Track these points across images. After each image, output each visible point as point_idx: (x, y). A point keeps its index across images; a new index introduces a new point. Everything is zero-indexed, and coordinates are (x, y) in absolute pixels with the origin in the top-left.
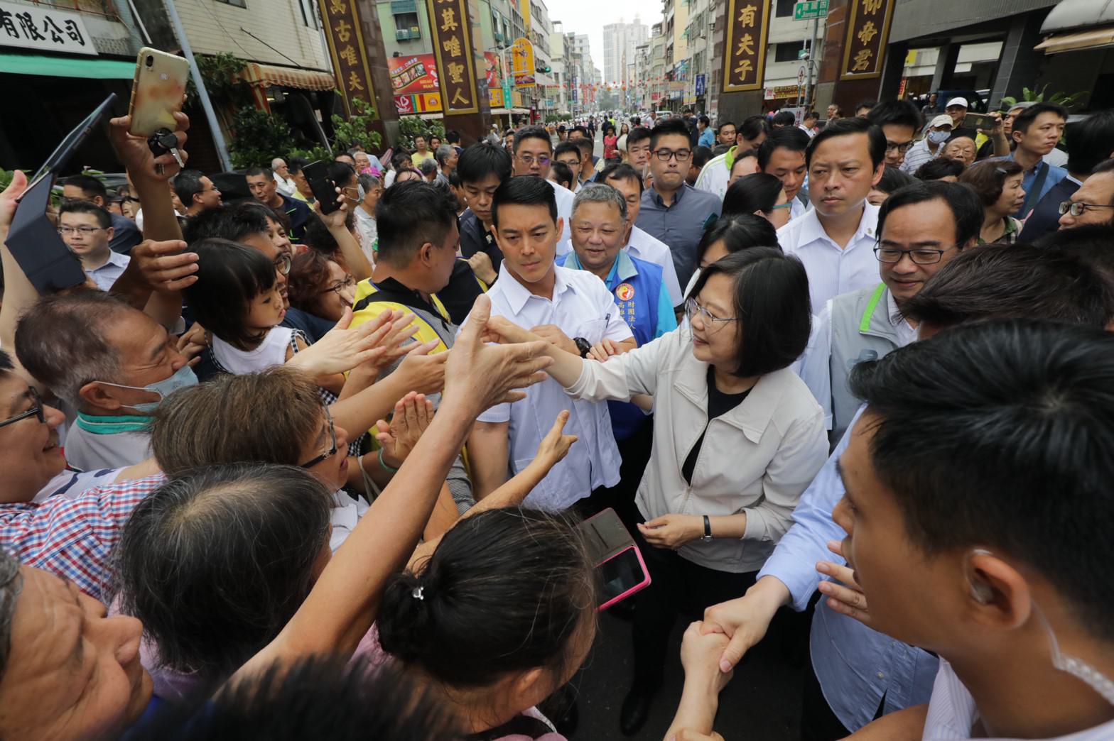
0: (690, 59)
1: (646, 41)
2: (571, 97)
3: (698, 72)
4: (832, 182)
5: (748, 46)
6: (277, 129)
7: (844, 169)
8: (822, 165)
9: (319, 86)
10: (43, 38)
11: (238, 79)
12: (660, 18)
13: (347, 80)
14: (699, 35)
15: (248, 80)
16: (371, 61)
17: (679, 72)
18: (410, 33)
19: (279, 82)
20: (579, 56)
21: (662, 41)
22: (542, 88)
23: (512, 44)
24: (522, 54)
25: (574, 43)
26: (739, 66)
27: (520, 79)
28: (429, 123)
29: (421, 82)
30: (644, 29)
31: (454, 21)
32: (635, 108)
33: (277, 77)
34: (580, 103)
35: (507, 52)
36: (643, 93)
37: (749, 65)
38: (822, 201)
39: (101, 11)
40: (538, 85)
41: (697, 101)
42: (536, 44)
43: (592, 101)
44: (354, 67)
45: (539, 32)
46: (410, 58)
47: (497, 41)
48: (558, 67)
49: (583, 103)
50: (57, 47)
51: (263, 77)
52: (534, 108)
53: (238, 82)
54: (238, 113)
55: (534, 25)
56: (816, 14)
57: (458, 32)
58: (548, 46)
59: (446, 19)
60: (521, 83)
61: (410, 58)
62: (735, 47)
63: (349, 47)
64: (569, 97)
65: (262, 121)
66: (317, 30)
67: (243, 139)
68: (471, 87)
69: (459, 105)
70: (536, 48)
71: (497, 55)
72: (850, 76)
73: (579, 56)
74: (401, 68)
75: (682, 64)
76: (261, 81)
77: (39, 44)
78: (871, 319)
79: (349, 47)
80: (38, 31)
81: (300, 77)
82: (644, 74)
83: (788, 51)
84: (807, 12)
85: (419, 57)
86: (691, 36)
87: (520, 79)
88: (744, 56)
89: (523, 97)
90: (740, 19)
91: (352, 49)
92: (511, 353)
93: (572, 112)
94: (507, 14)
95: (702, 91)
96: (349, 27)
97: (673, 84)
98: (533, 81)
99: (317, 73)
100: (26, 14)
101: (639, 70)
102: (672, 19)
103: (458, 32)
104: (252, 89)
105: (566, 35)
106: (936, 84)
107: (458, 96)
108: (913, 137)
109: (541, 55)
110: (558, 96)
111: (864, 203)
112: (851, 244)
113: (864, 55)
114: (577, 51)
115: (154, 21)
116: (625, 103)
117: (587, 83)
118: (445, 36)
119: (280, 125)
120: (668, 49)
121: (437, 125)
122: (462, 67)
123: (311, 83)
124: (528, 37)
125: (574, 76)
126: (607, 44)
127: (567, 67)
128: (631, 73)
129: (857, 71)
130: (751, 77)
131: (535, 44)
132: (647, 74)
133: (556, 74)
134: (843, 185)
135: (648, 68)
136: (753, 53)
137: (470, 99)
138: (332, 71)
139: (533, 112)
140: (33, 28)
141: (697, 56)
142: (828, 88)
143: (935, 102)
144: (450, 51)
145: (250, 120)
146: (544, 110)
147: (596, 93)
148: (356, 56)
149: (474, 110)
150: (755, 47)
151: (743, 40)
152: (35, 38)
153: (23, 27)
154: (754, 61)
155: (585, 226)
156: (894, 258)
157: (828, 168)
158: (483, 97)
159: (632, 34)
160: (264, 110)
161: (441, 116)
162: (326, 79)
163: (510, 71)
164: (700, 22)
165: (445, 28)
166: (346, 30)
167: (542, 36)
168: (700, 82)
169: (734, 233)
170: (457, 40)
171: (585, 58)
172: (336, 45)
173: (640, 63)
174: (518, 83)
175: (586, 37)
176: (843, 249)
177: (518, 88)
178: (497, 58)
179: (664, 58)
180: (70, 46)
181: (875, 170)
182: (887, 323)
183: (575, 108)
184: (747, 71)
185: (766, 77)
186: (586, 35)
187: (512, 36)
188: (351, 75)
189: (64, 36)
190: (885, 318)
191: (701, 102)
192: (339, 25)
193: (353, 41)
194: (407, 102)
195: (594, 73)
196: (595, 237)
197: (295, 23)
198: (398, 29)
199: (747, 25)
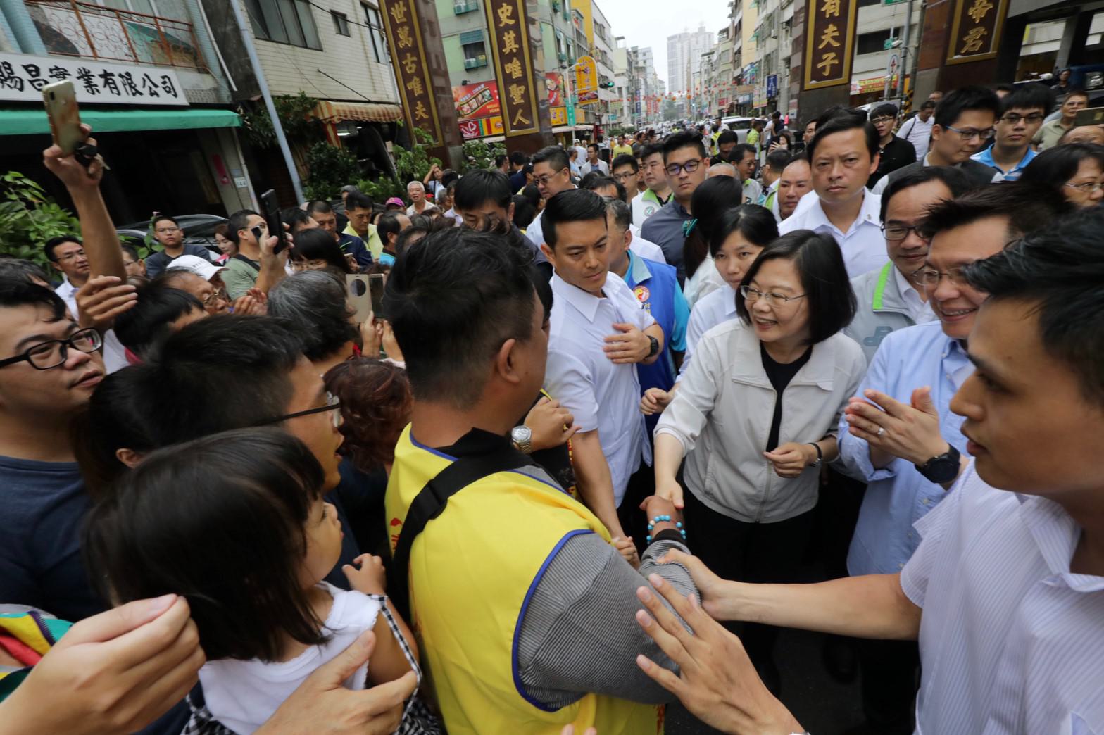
0: (760, 61)
1: (712, 47)
2: (635, 110)
3: (768, 74)
4: (835, 172)
5: (833, 38)
6: (347, 162)
7: (846, 160)
8: (825, 159)
9: (387, 118)
10: (141, 94)
11: (312, 117)
12: (727, 23)
13: (413, 110)
14: (770, 35)
15: (321, 118)
16: (436, 90)
18: (477, 61)
19: (349, 117)
20: (643, 69)
21: (729, 45)
22: (605, 103)
23: (575, 62)
24: (585, 71)
25: (637, 56)
27: (583, 97)
28: (492, 145)
29: (488, 107)
30: (710, 36)
31: (515, 43)
33: (348, 113)
34: (644, 115)
35: (571, 71)
36: (710, 100)
37: (834, 58)
38: (827, 190)
39: (193, 65)
40: (601, 100)
41: (768, 103)
42: (599, 61)
43: (655, 112)
44: (421, 98)
46: (479, 84)
47: (561, 61)
48: (621, 82)
49: (647, 114)
51: (335, 113)
52: (598, 124)
53: (312, 120)
54: (310, 149)
55: (598, 42)
57: (519, 54)
58: (611, 62)
60: (584, 100)
61: (479, 84)
62: (818, 40)
63: (415, 78)
64: (633, 109)
65: (332, 155)
67: (315, 174)
68: (532, 107)
70: (599, 65)
71: (561, 74)
73: (643, 69)
74: (469, 95)
76: (332, 117)
78: (883, 297)
79: (415, 78)
80: (137, 88)
81: (370, 111)
82: (710, 81)
83: (873, 42)
85: (486, 83)
86: (761, 36)
87: (583, 97)
88: (829, 48)
89: (586, 113)
90: (823, 9)
91: (418, 79)
92: (563, 419)
93: (636, 124)
94: (571, 34)
95: (773, 93)
96: (415, 59)
97: (741, 88)
98: (596, 97)
99: (387, 106)
100: (128, 74)
101: (705, 77)
102: (740, 22)
103: (519, 54)
104: (325, 126)
105: (630, 50)
106: (1061, 62)
107: (519, 117)
108: (993, 122)
109: (604, 71)
110: (622, 110)
111: (864, 190)
112: (852, 229)
113: (975, 35)
114: (641, 64)
115: (240, 70)
116: (690, 112)
117: (651, 96)
118: (506, 59)
119: (348, 159)
120: (736, 53)
121: (499, 148)
122: (523, 88)
124: (591, 55)
125: (637, 89)
126: (671, 54)
127: (630, 80)
128: (696, 82)
129: (967, 53)
130: (837, 71)
131: (598, 61)
132: (713, 80)
133: (620, 89)
134: (845, 175)
135: (714, 74)
136: (838, 45)
138: (400, 102)
139: (597, 127)
141: (768, 57)
142: (930, 76)
143: (1066, 81)
144: (511, 73)
145: (321, 155)
146: (607, 125)
147: (660, 104)
149: (535, 130)
150: (841, 38)
151: (826, 31)
152: (134, 94)
153: (124, 85)
154: (840, 53)
156: (901, 236)
157: (831, 161)
158: (543, 116)
159: (697, 43)
160: (336, 144)
161: (502, 138)
162: (394, 111)
163: (573, 89)
164: (770, 22)
166: (413, 62)
167: (605, 53)
168: (772, 84)
169: (746, 221)
171: (648, 70)
172: (403, 78)
174: (581, 100)
176: (845, 233)
177: (582, 105)
178: (561, 77)
181: (872, 161)
182: (899, 299)
183: (639, 121)
184: (832, 66)
185: (854, 71)
186: (649, 48)
187: (575, 55)
188: (417, 105)
189: (160, 91)
190: (897, 295)
191: (772, 103)
192: (406, 58)
195: (658, 84)
197: (368, 61)
198: (467, 58)
199: (832, 14)
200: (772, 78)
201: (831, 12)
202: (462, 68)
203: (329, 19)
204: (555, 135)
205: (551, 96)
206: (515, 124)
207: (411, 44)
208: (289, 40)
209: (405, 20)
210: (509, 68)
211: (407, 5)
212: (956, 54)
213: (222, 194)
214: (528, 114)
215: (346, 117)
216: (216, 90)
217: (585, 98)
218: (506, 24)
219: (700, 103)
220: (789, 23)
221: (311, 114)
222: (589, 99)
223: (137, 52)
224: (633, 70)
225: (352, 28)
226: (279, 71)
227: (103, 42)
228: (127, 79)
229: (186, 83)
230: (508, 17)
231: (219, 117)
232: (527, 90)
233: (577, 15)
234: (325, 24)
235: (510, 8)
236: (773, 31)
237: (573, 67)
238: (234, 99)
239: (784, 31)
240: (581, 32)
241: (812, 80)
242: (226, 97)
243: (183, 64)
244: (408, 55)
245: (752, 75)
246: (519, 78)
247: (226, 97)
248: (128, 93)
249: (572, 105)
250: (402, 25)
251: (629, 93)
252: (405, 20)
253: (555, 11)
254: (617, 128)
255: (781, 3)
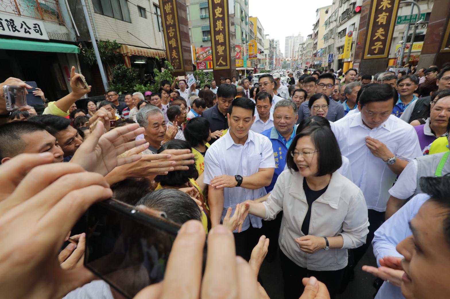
2: (271, 63)
3: (329, 53)
5: (382, 35)
10: (19, 31)
11: (118, 52)
12: (311, 32)
14: (331, 38)
15: (122, 53)
17: (320, 53)
20: (275, 48)
21: (311, 41)
22: (259, 60)
23: (249, 42)
24: (253, 46)
25: (273, 43)
26: (374, 45)
31: (222, 26)
32: (297, 68)
34: (274, 66)
35: (246, 45)
36: (302, 62)
39: (57, 21)
40: (258, 59)
44: (175, 48)
45: (260, 38)
47: (243, 41)
48: (267, 52)
49: (276, 66)
50: (27, 35)
51: (129, 51)
52: (256, 68)
55: (258, 35)
56: (409, 21)
58: (263, 44)
59: (218, 25)
60: (251, 57)
62: (373, 35)
63: (173, 39)
64: (270, 63)
66: (160, 31)
69: (221, 65)
70: (258, 44)
71: (242, 46)
72: (446, 50)
74: (203, 51)
75: (321, 50)
76: (128, 53)
77: (16, 34)
79: (173, 39)
82: (302, 55)
84: (404, 20)
86: (326, 38)
87: (251, 56)
88: (378, 40)
89: (251, 63)
90: (377, 20)
91: (174, 40)
93: (271, 69)
96: (174, 30)
98: (256, 57)
100: (11, 20)
101: (300, 53)
102: (317, 32)
104: (124, 57)
105: (271, 40)
107: (221, 61)
110: (266, 63)
114: (275, 46)
115: (86, 27)
120: (315, 44)
122: (224, 47)
123: (154, 54)
125: (273, 56)
126: (287, 43)
127: (270, 52)
130: (381, 51)
131: (258, 43)
132: (304, 55)
133: (266, 55)
135: (304, 52)
137: (226, 62)
138: (165, 49)
139: (255, 69)
140: (14, 26)
144: (218, 40)
148: (176, 43)
149: (228, 67)
151: (378, 31)
152: (14, 31)
153: (8, 26)
155: (278, 116)
158: (232, 62)
159: (297, 40)
162: (162, 53)
165: (217, 29)
166: (173, 31)
167: (261, 40)
168: (331, 57)
170: (222, 35)
171: (277, 49)
172: (168, 38)
173: (300, 51)
174: (250, 57)
175: (278, 41)
178: (242, 48)
179: (312, 48)
180: (34, 35)
184: (379, 48)
187: (249, 39)
189: (32, 31)
193: (175, 36)
194: (204, 65)
196: (283, 121)
199: (382, 23)
200: (331, 55)
201: (382, 22)
202: (202, 40)
203: (137, 9)
204: (237, 71)
205: (237, 55)
206: (218, 64)
207: (174, 23)
208: (114, 16)
209: (170, 12)
210: (218, 37)
211: (172, 4)
212: (446, 48)
213: (68, 86)
214: (225, 60)
215: (135, 53)
216: (68, 35)
217: (252, 57)
218: (218, 17)
219: (297, 63)
220: (339, 33)
221: (118, 51)
222: (253, 57)
223: (21, 10)
224: (272, 48)
225: (148, 14)
226: (103, 29)
227: (8, 5)
228: (11, 23)
229: (49, 28)
230: (219, 14)
231: (66, 47)
232: (225, 49)
233: (251, 23)
234: (134, 12)
235: (221, 9)
236: (332, 36)
237: (248, 44)
238: (77, 40)
239: (337, 36)
240: (252, 30)
241: (368, 54)
242: (73, 38)
243: (50, 20)
244: (171, 28)
245: (321, 53)
246: (222, 42)
247: (73, 38)
248: (10, 30)
249: (246, 59)
250: (169, 14)
251: (269, 56)
252: (170, 12)
253: (242, 20)
254: (264, 70)
255: (337, 25)
